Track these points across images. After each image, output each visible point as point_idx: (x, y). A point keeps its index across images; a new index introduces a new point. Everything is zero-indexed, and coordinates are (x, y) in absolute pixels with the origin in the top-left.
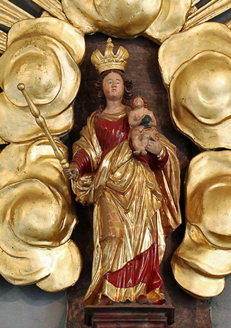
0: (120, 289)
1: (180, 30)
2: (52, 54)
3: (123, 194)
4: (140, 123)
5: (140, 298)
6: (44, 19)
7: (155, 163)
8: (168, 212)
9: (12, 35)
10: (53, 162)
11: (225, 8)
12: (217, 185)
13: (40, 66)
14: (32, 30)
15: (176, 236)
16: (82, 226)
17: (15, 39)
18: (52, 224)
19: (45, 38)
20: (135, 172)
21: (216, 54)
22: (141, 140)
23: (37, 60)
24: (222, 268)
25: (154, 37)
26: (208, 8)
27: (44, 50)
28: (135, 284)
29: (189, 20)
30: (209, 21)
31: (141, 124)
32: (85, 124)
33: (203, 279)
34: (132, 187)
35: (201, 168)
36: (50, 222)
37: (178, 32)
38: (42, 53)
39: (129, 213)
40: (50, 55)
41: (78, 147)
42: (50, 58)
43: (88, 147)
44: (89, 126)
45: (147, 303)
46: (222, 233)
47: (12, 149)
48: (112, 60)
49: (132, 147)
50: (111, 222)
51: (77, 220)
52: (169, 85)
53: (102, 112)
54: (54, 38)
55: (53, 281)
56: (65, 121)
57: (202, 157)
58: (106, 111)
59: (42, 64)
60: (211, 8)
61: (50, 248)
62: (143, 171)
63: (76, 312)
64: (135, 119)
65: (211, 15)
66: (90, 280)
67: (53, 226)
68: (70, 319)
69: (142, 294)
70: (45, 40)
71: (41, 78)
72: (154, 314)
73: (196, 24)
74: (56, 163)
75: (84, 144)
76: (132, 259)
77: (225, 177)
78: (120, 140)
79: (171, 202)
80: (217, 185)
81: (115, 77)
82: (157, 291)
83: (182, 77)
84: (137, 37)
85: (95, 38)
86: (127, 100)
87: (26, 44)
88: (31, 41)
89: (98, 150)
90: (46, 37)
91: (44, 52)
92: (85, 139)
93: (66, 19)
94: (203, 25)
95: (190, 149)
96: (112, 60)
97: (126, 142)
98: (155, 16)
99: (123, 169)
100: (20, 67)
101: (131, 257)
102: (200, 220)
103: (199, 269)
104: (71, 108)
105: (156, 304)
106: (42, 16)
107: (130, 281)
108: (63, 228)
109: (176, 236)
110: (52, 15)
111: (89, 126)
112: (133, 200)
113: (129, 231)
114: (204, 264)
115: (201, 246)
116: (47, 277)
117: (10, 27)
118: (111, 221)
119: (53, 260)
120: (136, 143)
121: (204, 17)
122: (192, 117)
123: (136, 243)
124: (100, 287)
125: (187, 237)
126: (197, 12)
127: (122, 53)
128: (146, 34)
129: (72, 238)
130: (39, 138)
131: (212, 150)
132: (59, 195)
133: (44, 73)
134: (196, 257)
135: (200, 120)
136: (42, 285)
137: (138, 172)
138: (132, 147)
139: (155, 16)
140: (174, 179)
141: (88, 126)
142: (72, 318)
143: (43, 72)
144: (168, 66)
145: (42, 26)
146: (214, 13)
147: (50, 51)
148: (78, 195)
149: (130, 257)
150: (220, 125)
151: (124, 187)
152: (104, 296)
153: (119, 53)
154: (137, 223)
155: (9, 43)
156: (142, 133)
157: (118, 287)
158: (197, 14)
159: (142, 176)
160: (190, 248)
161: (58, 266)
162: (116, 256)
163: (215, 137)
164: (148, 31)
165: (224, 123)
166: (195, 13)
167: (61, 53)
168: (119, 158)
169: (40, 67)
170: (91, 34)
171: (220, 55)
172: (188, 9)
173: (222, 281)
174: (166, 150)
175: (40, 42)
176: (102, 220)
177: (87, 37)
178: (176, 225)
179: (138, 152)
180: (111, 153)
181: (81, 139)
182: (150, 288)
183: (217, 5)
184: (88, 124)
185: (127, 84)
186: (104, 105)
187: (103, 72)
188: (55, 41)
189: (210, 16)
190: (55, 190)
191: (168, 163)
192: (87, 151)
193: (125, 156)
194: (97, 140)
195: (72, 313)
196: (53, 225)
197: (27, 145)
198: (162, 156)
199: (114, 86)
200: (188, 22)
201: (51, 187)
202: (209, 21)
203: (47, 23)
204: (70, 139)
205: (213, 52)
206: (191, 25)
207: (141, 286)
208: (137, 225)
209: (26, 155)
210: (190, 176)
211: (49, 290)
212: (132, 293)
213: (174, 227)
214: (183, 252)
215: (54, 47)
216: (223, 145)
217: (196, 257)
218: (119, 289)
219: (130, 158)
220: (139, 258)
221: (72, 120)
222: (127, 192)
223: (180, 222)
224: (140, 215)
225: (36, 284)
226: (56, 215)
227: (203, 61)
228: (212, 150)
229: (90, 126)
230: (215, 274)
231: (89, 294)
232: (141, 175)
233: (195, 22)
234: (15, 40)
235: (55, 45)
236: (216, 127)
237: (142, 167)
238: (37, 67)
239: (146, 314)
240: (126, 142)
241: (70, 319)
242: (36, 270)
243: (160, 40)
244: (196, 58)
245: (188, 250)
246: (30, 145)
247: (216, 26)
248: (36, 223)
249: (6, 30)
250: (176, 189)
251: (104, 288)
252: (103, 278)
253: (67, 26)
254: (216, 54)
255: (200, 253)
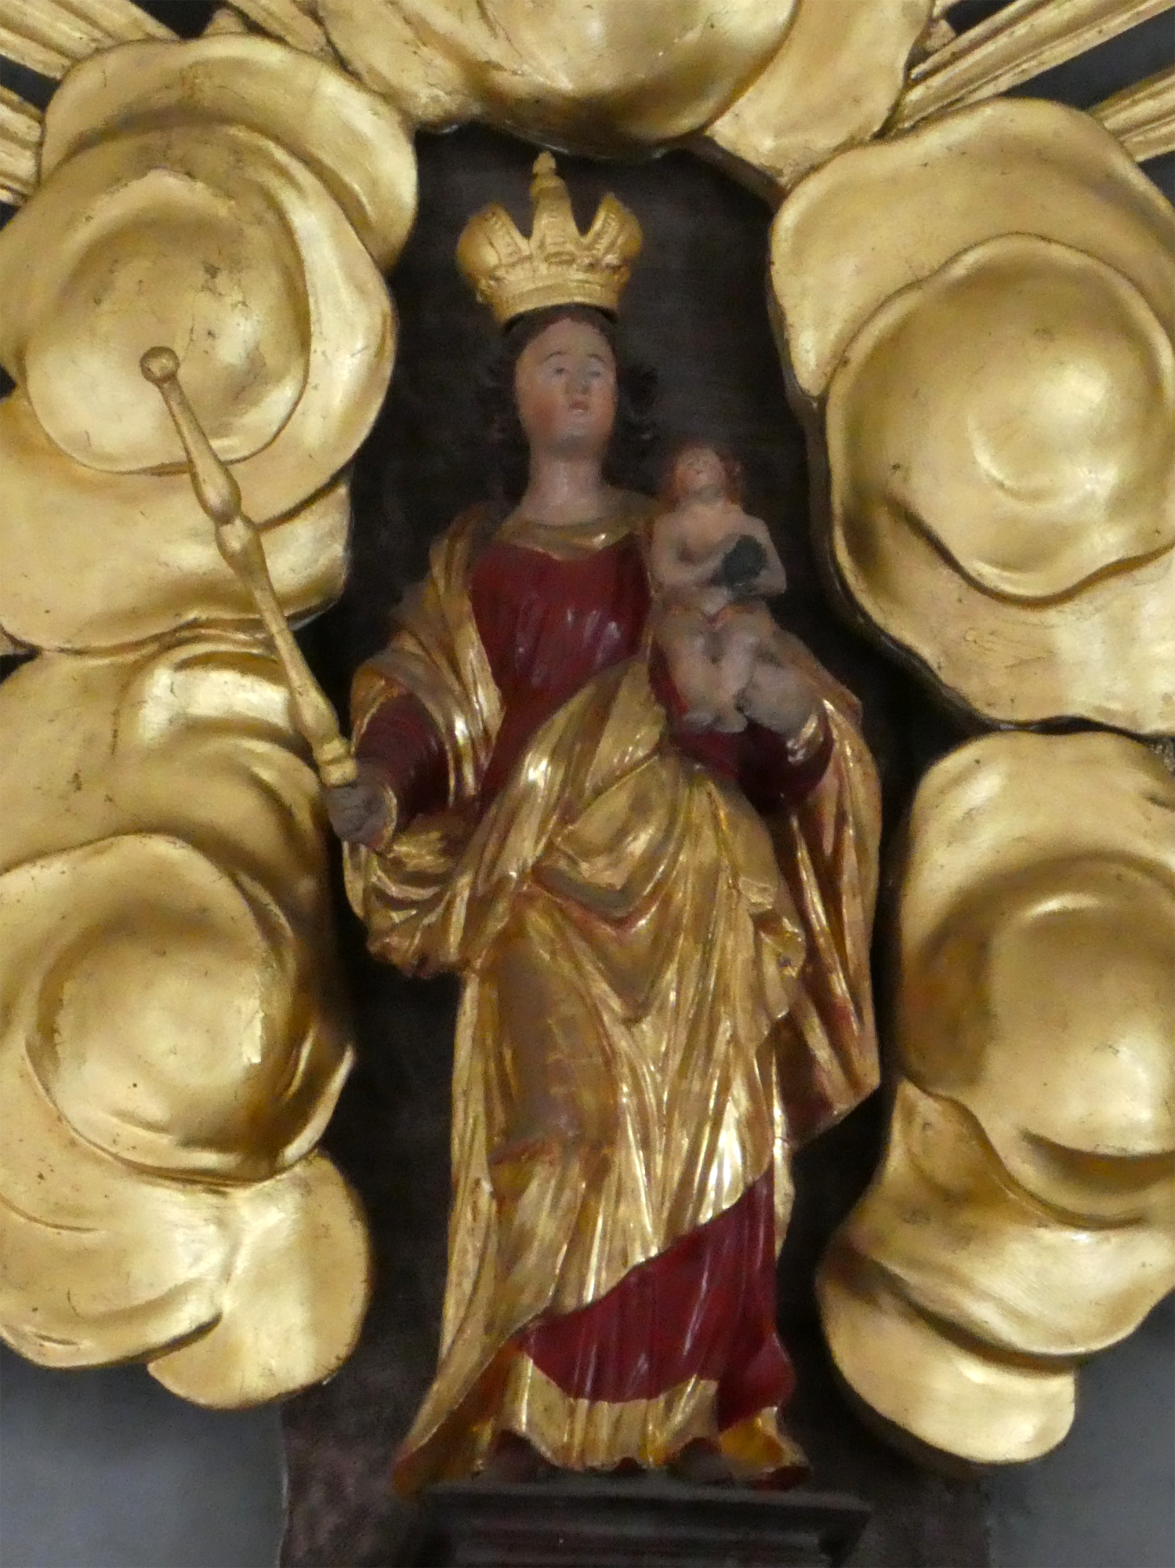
0: (590, 1410)
1: (876, 129)
2: (270, 217)
3: (622, 923)
4: (710, 575)
5: (690, 1456)
6: (222, 45)
7: (767, 778)
8: (813, 1029)
9: (68, 113)
10: (251, 752)
11: (1087, 36)
12: (1052, 905)
13: (212, 271)
14: (171, 97)
15: (840, 1155)
16: (381, 1083)
17: (81, 135)
18: (245, 1061)
19: (234, 138)
20: (681, 818)
21: (1056, 252)
22: (715, 660)
23: (202, 248)
24: (1067, 1321)
25: (752, 157)
26: (1007, 32)
27: (229, 195)
28: (663, 1380)
29: (917, 82)
30: (1015, 93)
31: (715, 581)
32: (419, 568)
33: (976, 1373)
34: (663, 894)
35: (979, 813)
36: (241, 1054)
37: (868, 138)
38: (222, 209)
39: (645, 1026)
40: (260, 221)
41: (383, 683)
42: (258, 237)
43: (438, 689)
44: (441, 584)
45: (724, 1481)
46: (1084, 1145)
47: (46, 686)
48: (540, 259)
49: (664, 687)
50: (559, 1061)
51: (358, 1053)
52: (823, 400)
53: (505, 514)
54: (277, 140)
55: (229, 1354)
56: (308, 552)
57: (978, 762)
58: (528, 510)
59: (222, 265)
60: (1021, 29)
61: (222, 1189)
62: (715, 817)
63: (330, 1521)
64: (686, 556)
65: (1024, 66)
66: (425, 1360)
67: (253, 1074)
68: (300, 1554)
69: (698, 1431)
70: (238, 152)
71: (216, 331)
72: (774, 1537)
73: (949, 107)
74: (272, 764)
75: (418, 670)
76: (654, 1252)
77: (1115, 869)
78: (600, 657)
79: (834, 977)
80: (1052, 905)
81: (579, 342)
82: (767, 1421)
83: (890, 362)
84: (664, 157)
85: (476, 151)
86: (634, 462)
87: (145, 164)
88: (169, 147)
89: (486, 699)
90: (240, 133)
91: (233, 203)
92: (420, 643)
93: (329, 49)
94: (988, 111)
95: (917, 721)
96: (540, 259)
97: (640, 669)
98: (764, 59)
99: (618, 801)
100: (112, 272)
101: (647, 1246)
102: (972, 1075)
103: (961, 1321)
104: (342, 491)
105: (756, 1485)
106: (209, 30)
107: (642, 1364)
108: (293, 1088)
109: (840, 1155)
110: (254, 28)
111: (441, 584)
112: (668, 956)
113: (642, 1110)
114: (984, 1296)
115: (976, 1196)
116: (202, 1330)
117: (58, 76)
118: (559, 1056)
119: (234, 1249)
120: (692, 670)
121: (987, 73)
122: (935, 557)
123: (677, 1174)
124: (491, 1388)
125: (896, 1162)
126: (954, 47)
127: (613, 231)
128: (711, 142)
129: (330, 1144)
130: (186, 634)
131: (1024, 727)
132: (283, 920)
133: (234, 306)
134: (946, 1257)
135: (973, 574)
136: (169, 1375)
137: (695, 816)
138: (664, 687)
139: (764, 59)
140: (850, 859)
141: (434, 584)
142: (310, 1551)
143: (228, 300)
144: (820, 301)
145: (217, 81)
146: (1034, 57)
147: (258, 204)
148: (379, 921)
149: (645, 1249)
150: (1068, 607)
151: (627, 892)
152: (512, 1443)
153: (603, 226)
154: (683, 1072)
155: (50, 158)
156: (719, 626)
157: (578, 1394)
158: (956, 57)
159: (715, 833)
160: (915, 1214)
161: (250, 1288)
162: (578, 1236)
163: (1045, 658)
164: (725, 132)
165: (1086, 596)
166: (945, 54)
167: (313, 221)
168: (606, 744)
169: (214, 276)
170: (447, 131)
171: (1074, 260)
172: (916, 33)
173: (1063, 1387)
174: (824, 719)
175: (211, 156)
176: (508, 1055)
177: (432, 144)
178: (851, 1093)
179: (701, 717)
180: (561, 719)
181: (395, 644)
182: (732, 1408)
183: (1049, 17)
184: (437, 570)
185: (635, 385)
186: (517, 483)
187: (520, 318)
188: (281, 155)
189: (1018, 70)
190: (265, 898)
191: (829, 781)
192: (431, 706)
193: (630, 740)
194: (479, 652)
195: (312, 1529)
196: (253, 1066)
197: (122, 666)
198: (810, 743)
199: (568, 391)
200: (916, 94)
201: (245, 880)
202: (1015, 93)
203: (240, 66)
204: (337, 638)
205: (1043, 244)
206: (928, 106)
207: (695, 1394)
208: (684, 1085)
209: (116, 714)
210: (917, 857)
211: (205, 1396)
212: (666, 1420)
213: (842, 1105)
214: (882, 1225)
215: (274, 182)
216: (1079, 704)
217: (946, 1257)
218: (584, 1403)
219: (658, 749)
220: (687, 1247)
221: (346, 550)
222: (641, 917)
223: (872, 1079)
224: (703, 1035)
225: (144, 1367)
226: (267, 1022)
227: (991, 285)
228: (1024, 727)
229: (445, 586)
230: (1038, 1347)
231: (426, 1430)
232: (708, 833)
233: (947, 96)
234: (83, 144)
235: (283, 172)
236: (1052, 615)
237: (709, 794)
238: (201, 276)
239: (731, 1536)
240: (640, 669)
241: (300, 1554)
242: (152, 1295)
243: (780, 173)
244: (959, 270)
245: (906, 1221)
246: (136, 662)
247: (1044, 119)
248: (172, 1057)
249: (37, 91)
250: (855, 911)
251: (513, 1401)
252: (507, 1347)
253: (333, 85)
254: (1056, 252)
255: (964, 1238)
